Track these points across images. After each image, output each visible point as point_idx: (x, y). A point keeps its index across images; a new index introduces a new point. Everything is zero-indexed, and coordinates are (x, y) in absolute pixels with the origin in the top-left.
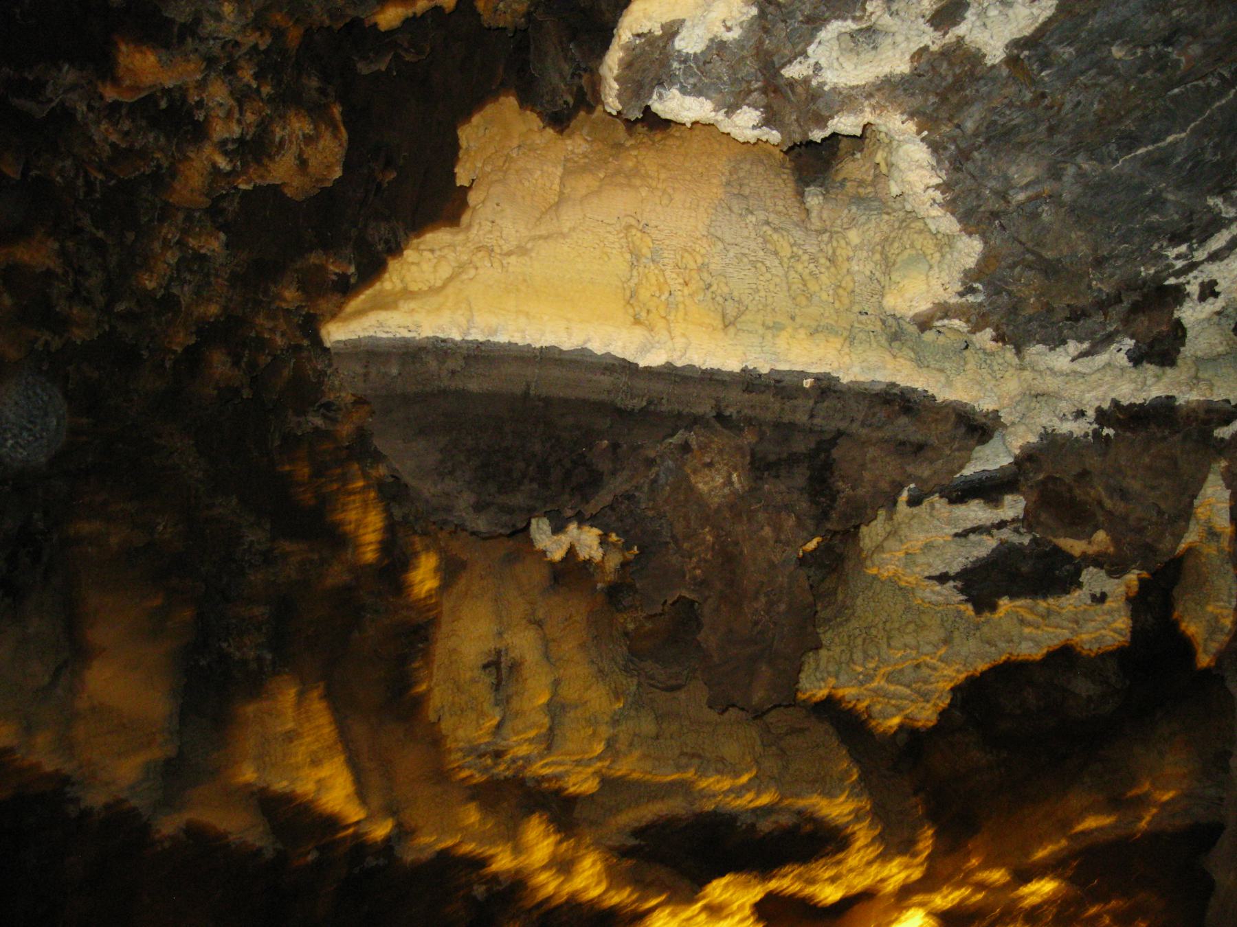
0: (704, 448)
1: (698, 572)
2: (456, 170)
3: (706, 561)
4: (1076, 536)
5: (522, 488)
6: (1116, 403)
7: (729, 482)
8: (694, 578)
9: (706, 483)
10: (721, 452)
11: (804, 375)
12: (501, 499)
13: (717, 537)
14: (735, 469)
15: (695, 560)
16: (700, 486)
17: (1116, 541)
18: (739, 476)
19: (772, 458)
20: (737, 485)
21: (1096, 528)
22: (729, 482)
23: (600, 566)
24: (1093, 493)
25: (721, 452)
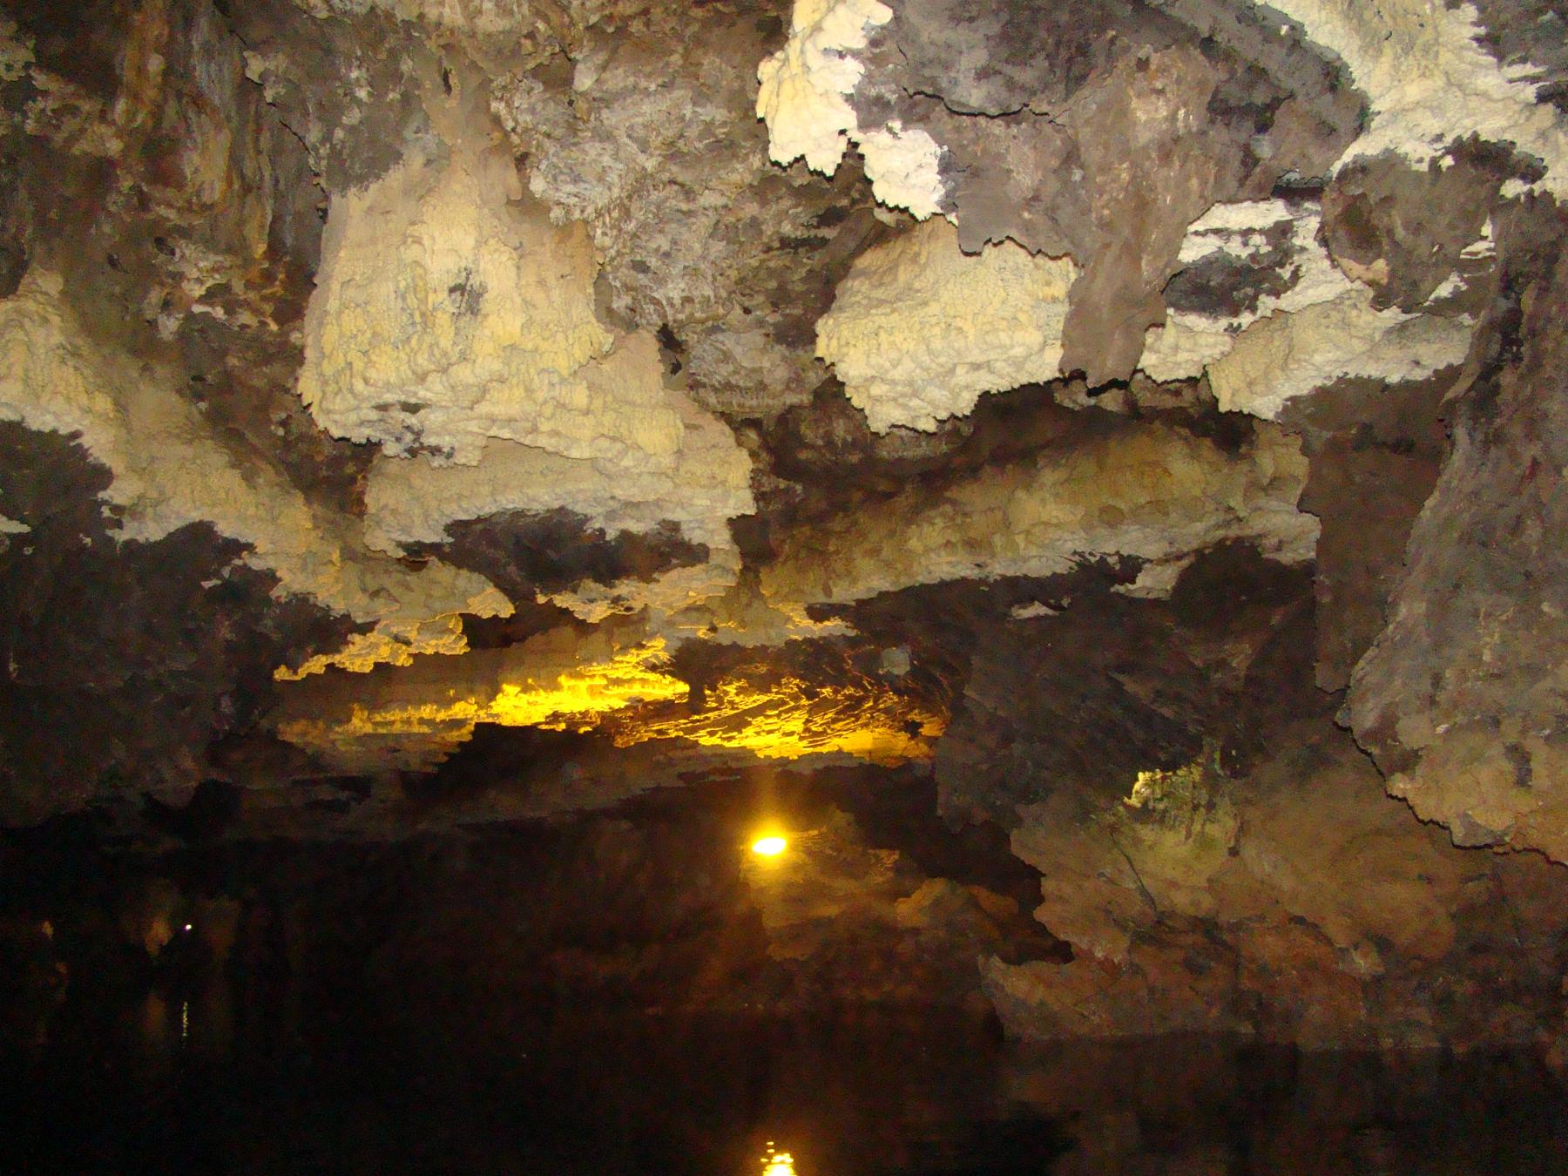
0: (1163, 70)
1: (1106, 212)
2: (34, 428)
3: (1117, 201)
4: (1357, 260)
5: (1033, 62)
6: (1475, 136)
7: (1173, 118)
8: (1100, 218)
9: (1147, 112)
10: (1178, 81)
11: (1285, 18)
12: (1009, 70)
13: (1134, 177)
14: (1185, 105)
15: (1106, 197)
16: (1139, 114)
17: (1392, 274)
18: (1187, 114)
19: (1233, 103)
20: (1180, 124)
21: (1379, 256)
22: (1173, 118)
23: (1456, 287)
24: (1386, 219)
25: (1178, 81)
